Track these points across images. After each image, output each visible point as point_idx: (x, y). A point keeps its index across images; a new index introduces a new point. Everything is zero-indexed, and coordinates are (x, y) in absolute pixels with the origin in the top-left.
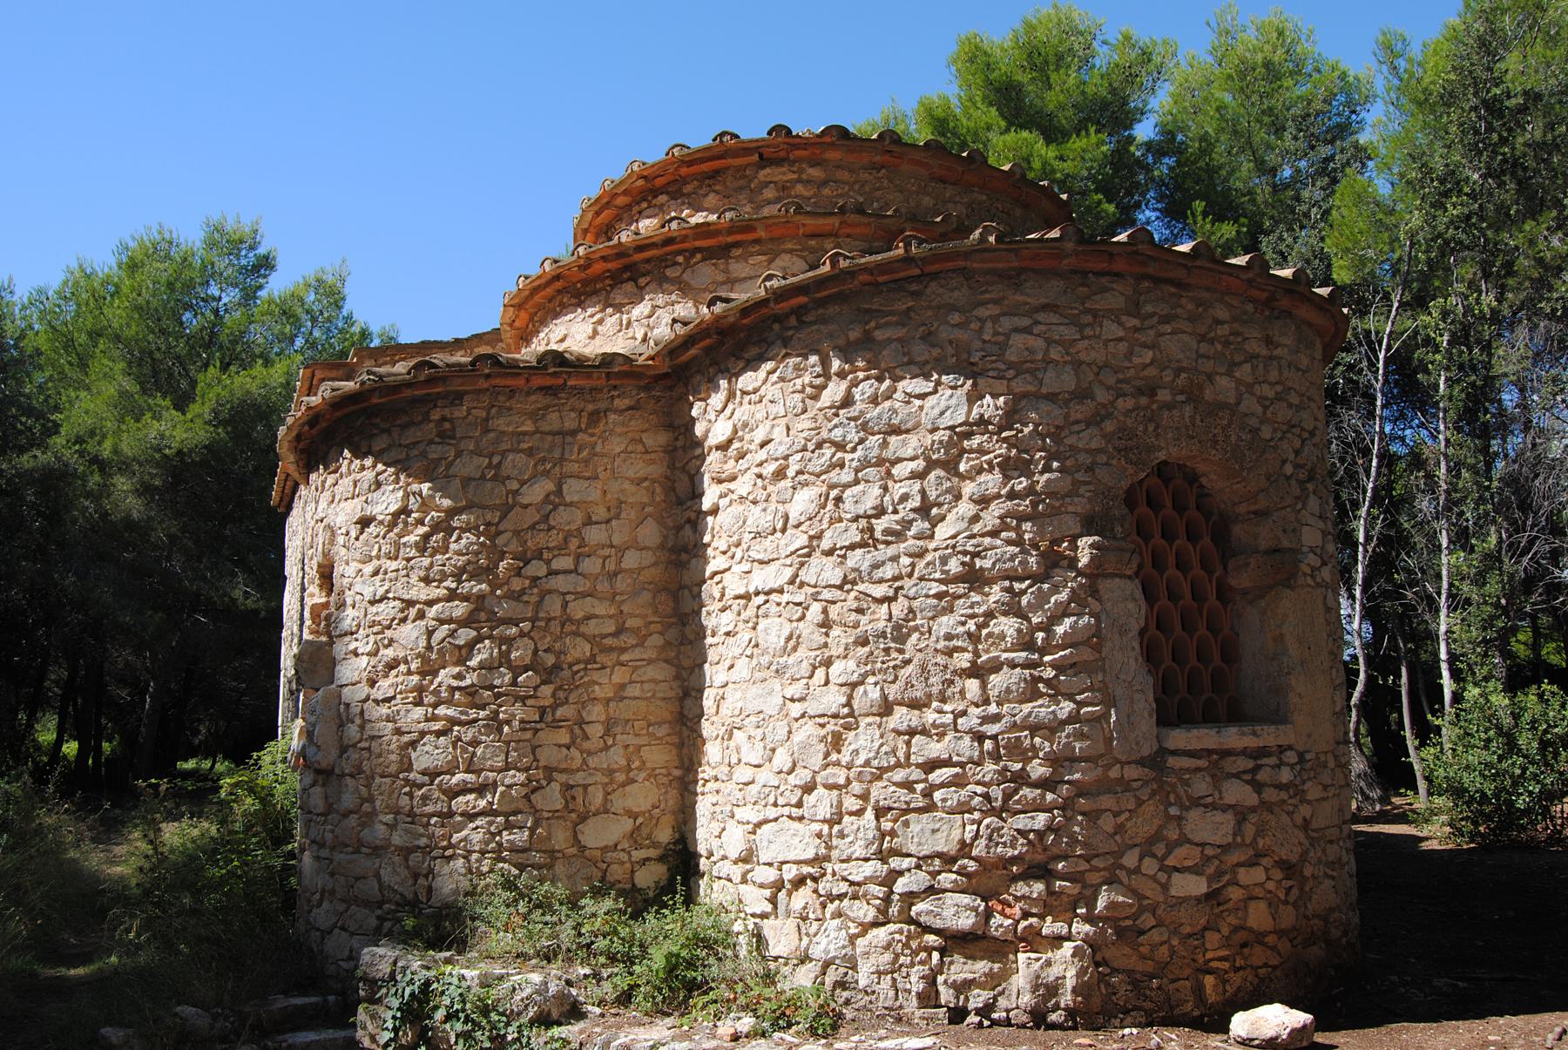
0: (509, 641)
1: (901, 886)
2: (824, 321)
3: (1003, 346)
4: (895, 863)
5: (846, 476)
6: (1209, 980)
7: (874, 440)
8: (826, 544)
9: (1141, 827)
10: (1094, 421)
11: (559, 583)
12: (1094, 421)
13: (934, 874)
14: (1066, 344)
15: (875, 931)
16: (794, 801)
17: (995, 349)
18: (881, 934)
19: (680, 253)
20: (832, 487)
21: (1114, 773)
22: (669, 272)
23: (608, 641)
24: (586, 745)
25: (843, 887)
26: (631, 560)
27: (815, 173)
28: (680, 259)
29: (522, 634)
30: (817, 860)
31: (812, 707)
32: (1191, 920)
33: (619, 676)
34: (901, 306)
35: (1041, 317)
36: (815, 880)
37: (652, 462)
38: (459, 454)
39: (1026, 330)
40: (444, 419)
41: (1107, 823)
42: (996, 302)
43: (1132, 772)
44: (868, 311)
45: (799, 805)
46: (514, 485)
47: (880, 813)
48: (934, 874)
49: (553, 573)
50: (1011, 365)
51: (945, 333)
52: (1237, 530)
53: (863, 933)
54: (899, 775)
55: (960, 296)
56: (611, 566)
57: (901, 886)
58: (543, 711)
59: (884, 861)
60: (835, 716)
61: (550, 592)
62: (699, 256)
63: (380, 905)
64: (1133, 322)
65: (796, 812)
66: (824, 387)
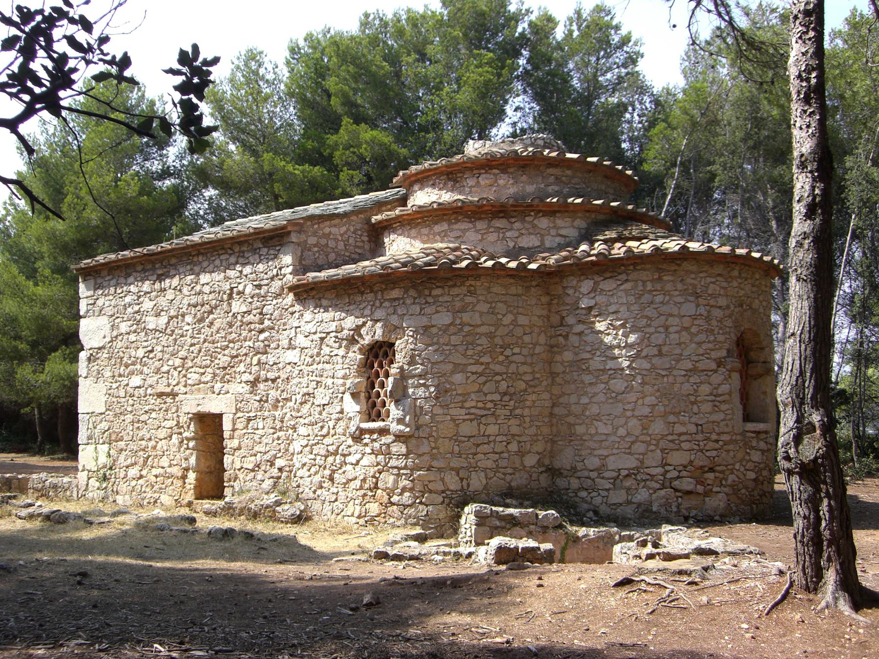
0: (497, 382)
1: (669, 476)
2: (644, 270)
3: (707, 287)
4: (667, 468)
5: (652, 330)
6: (754, 506)
7: (663, 318)
8: (644, 354)
9: (740, 455)
10: (730, 316)
11: (515, 358)
12: (730, 316)
13: (679, 471)
14: (725, 288)
15: (660, 491)
16: (627, 446)
17: (704, 289)
18: (662, 493)
19: (532, 211)
20: (646, 333)
21: (734, 438)
22: (527, 218)
23: (531, 383)
24: (525, 425)
25: (648, 477)
26: (538, 350)
27: (569, 172)
28: (532, 214)
29: (503, 380)
30: (637, 468)
31: (637, 413)
32: (751, 485)
33: (534, 397)
34: (673, 268)
35: (718, 278)
36: (635, 475)
37: (543, 309)
38: (478, 301)
39: (713, 283)
40: (471, 285)
41: (731, 453)
42: (706, 272)
43: (738, 437)
44: (661, 269)
45: (630, 448)
46: (500, 316)
47: (662, 450)
48: (679, 471)
49: (514, 354)
50: (709, 295)
51: (689, 281)
52: (752, 354)
53: (655, 492)
54: (670, 438)
55: (694, 268)
56: (531, 352)
57: (669, 476)
58: (511, 411)
59: (663, 467)
60: (647, 416)
61: (512, 362)
62: (541, 214)
63: (443, 492)
64: (740, 281)
65: (627, 451)
66: (643, 295)
